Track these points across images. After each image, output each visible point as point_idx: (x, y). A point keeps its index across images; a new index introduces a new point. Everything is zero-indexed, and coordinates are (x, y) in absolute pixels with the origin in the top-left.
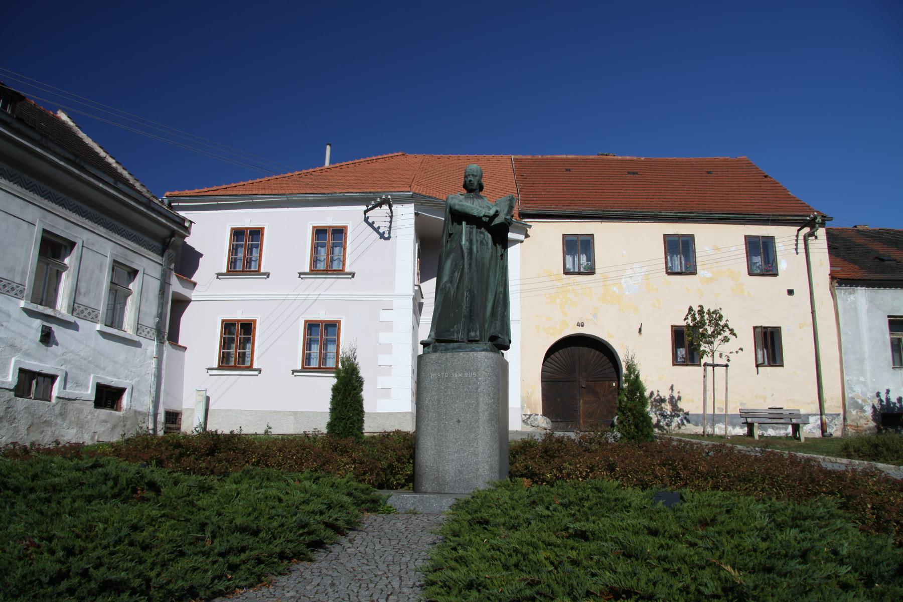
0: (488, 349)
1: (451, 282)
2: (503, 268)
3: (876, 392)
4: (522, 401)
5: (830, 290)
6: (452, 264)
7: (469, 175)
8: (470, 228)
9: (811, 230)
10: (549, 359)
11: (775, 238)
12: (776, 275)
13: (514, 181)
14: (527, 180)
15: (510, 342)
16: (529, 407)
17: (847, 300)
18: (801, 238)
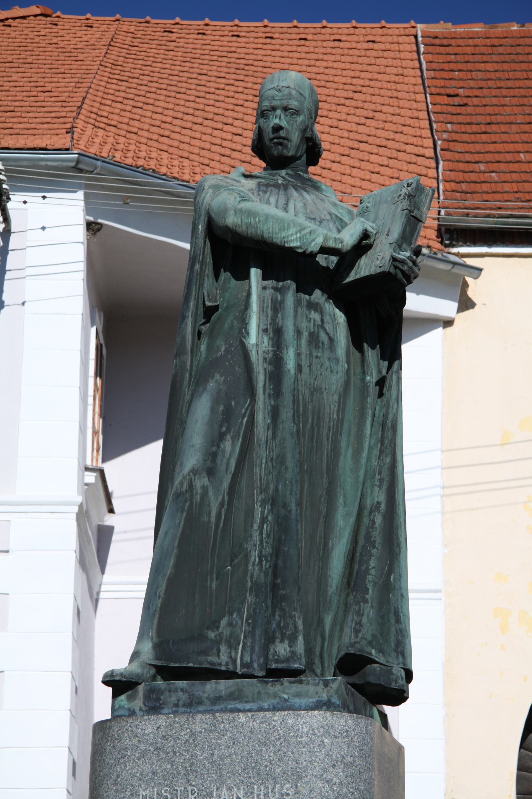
0: (335, 700)
1: (211, 472)
2: (383, 425)
6: (213, 410)
7: (274, 109)
8: (276, 289)
13: (424, 115)
14: (469, 110)
15: (409, 676)
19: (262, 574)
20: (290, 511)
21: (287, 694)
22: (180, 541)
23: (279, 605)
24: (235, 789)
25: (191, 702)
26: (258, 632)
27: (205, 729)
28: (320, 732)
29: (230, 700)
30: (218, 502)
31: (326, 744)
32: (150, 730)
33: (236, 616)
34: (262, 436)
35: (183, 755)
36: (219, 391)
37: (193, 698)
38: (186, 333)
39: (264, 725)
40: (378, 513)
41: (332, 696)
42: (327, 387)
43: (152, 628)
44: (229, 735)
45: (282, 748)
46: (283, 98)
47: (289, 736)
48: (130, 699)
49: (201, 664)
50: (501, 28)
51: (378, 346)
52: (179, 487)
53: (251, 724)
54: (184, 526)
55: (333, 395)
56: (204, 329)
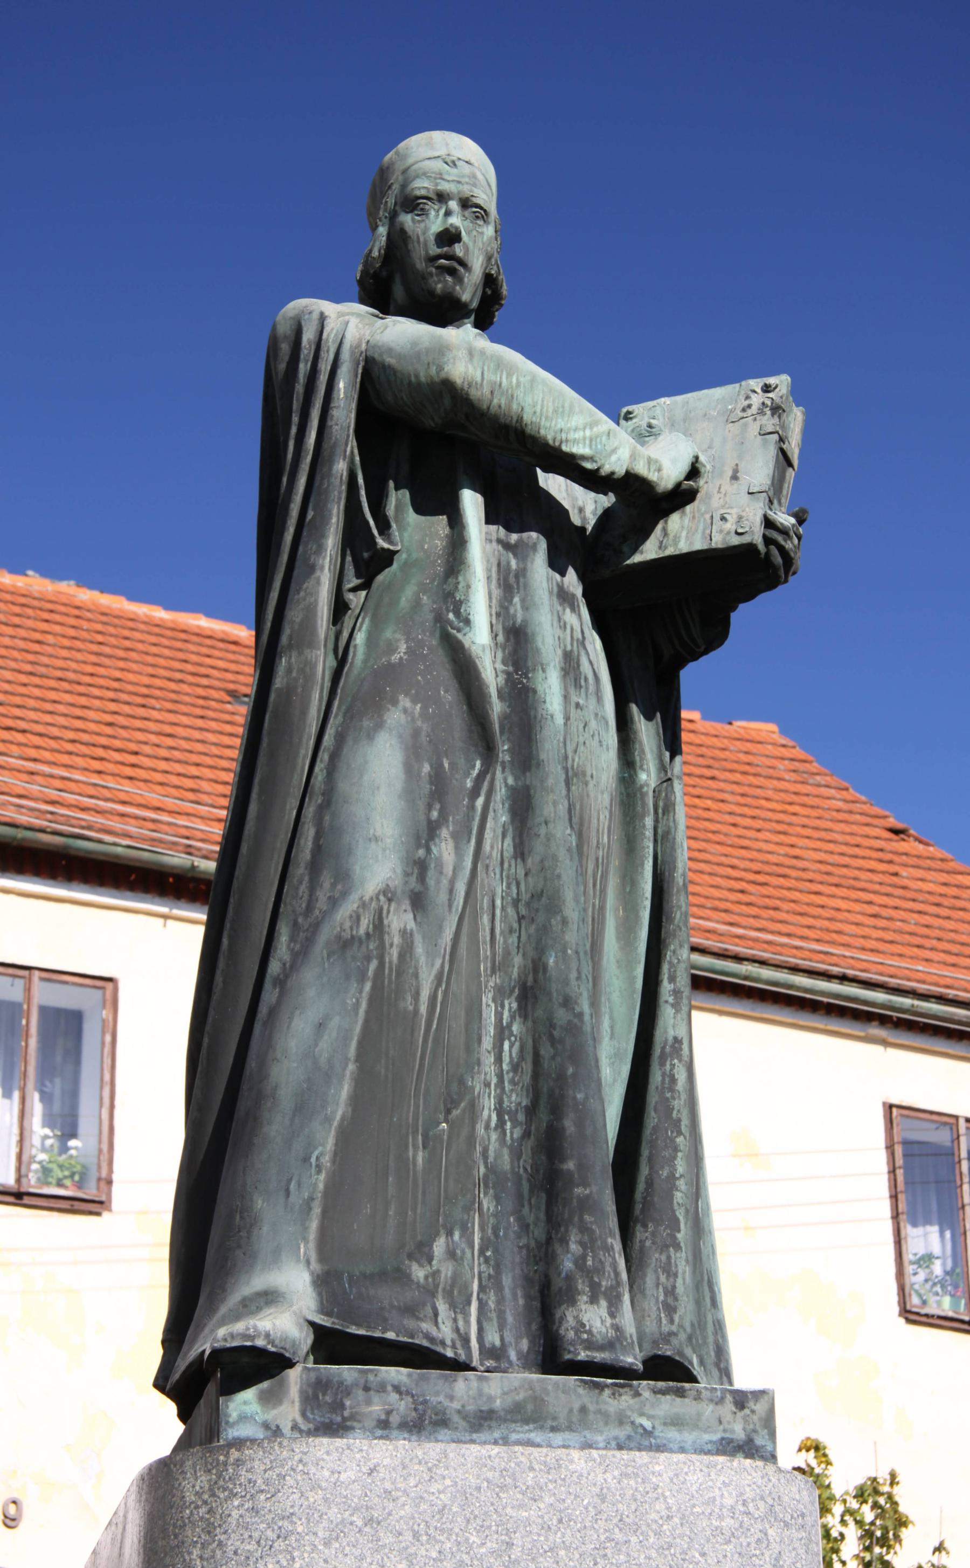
6: (410, 771)
7: (442, 197)
19: (506, 1151)
20: (580, 1015)
21: (649, 1417)
22: (360, 1044)
23: (576, 1219)
25: (421, 1418)
26: (507, 1280)
27: (488, 1481)
28: (758, 1509)
29: (515, 1422)
30: (435, 971)
31: (772, 1541)
33: (460, 1238)
34: (492, 847)
35: (437, 1541)
36: (416, 733)
37: (424, 1411)
38: (316, 601)
39: (632, 1482)
40: (680, 1061)
41: (754, 1431)
42: (594, 773)
43: (305, 1239)
44: (548, 1500)
45: (678, 1540)
46: (463, 180)
47: (692, 1513)
48: (268, 1399)
49: (412, 1337)
51: (658, 715)
52: (347, 924)
53: (600, 1478)
54: (367, 1012)
55: (602, 793)
56: (355, 600)
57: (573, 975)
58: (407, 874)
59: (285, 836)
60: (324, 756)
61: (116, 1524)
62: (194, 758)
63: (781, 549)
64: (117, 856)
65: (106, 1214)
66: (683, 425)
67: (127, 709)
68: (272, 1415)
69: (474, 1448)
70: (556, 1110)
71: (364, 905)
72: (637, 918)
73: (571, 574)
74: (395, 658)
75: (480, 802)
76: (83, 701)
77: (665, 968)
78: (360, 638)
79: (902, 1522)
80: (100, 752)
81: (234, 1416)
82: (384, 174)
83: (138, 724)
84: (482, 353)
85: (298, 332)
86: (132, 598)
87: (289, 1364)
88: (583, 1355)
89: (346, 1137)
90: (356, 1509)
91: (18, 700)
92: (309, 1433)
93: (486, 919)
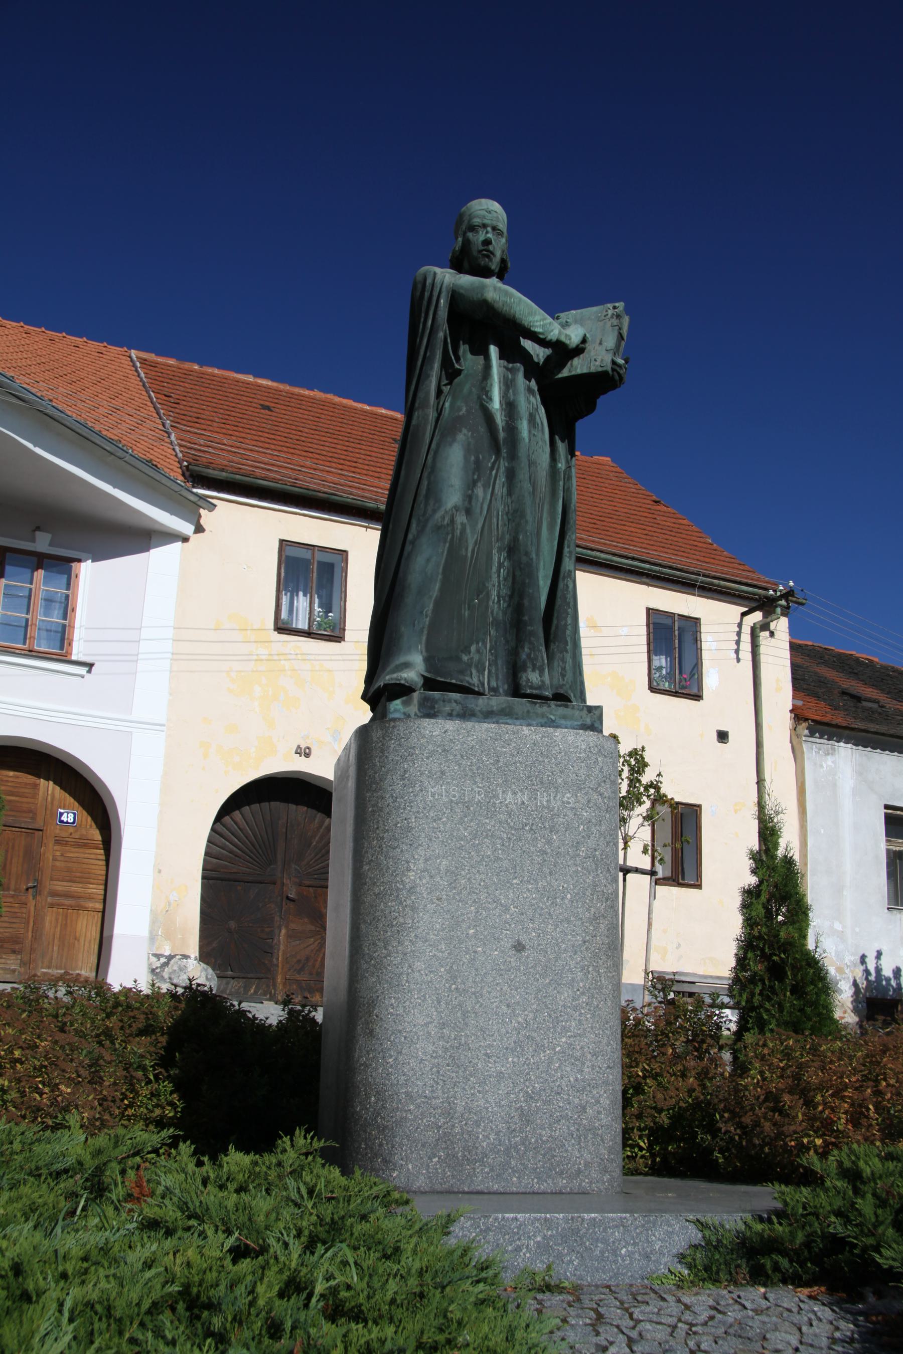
3: (861, 954)
4: (154, 921)
5: (791, 742)
6: (466, 459)
7: (484, 226)
9: (764, 617)
10: (227, 819)
11: (702, 622)
12: (697, 697)
16: (168, 936)
17: (821, 766)
18: (746, 630)
20: (532, 559)
24: (520, 794)
25: (465, 713)
26: (500, 662)
32: (437, 733)
36: (469, 444)
43: (421, 643)
48: (405, 704)
50: (187, 365)
57: (529, 543)
58: (464, 500)
59: (415, 483)
60: (432, 453)
61: (347, 749)
62: (379, 465)
63: (619, 373)
64: (348, 503)
65: (343, 643)
66: (580, 322)
67: (352, 445)
68: (407, 710)
69: (485, 725)
70: (521, 595)
71: (446, 512)
72: (556, 522)
73: (533, 383)
74: (461, 413)
75: (494, 472)
76: (335, 441)
77: (566, 542)
78: (447, 405)
79: (646, 765)
80: (342, 462)
81: (392, 709)
82: (461, 216)
83: (357, 451)
84: (500, 288)
85: (425, 280)
86: (355, 401)
87: (414, 691)
88: (529, 691)
89: (437, 603)
90: (439, 746)
91: (310, 440)
92: (421, 717)
93: (495, 520)
